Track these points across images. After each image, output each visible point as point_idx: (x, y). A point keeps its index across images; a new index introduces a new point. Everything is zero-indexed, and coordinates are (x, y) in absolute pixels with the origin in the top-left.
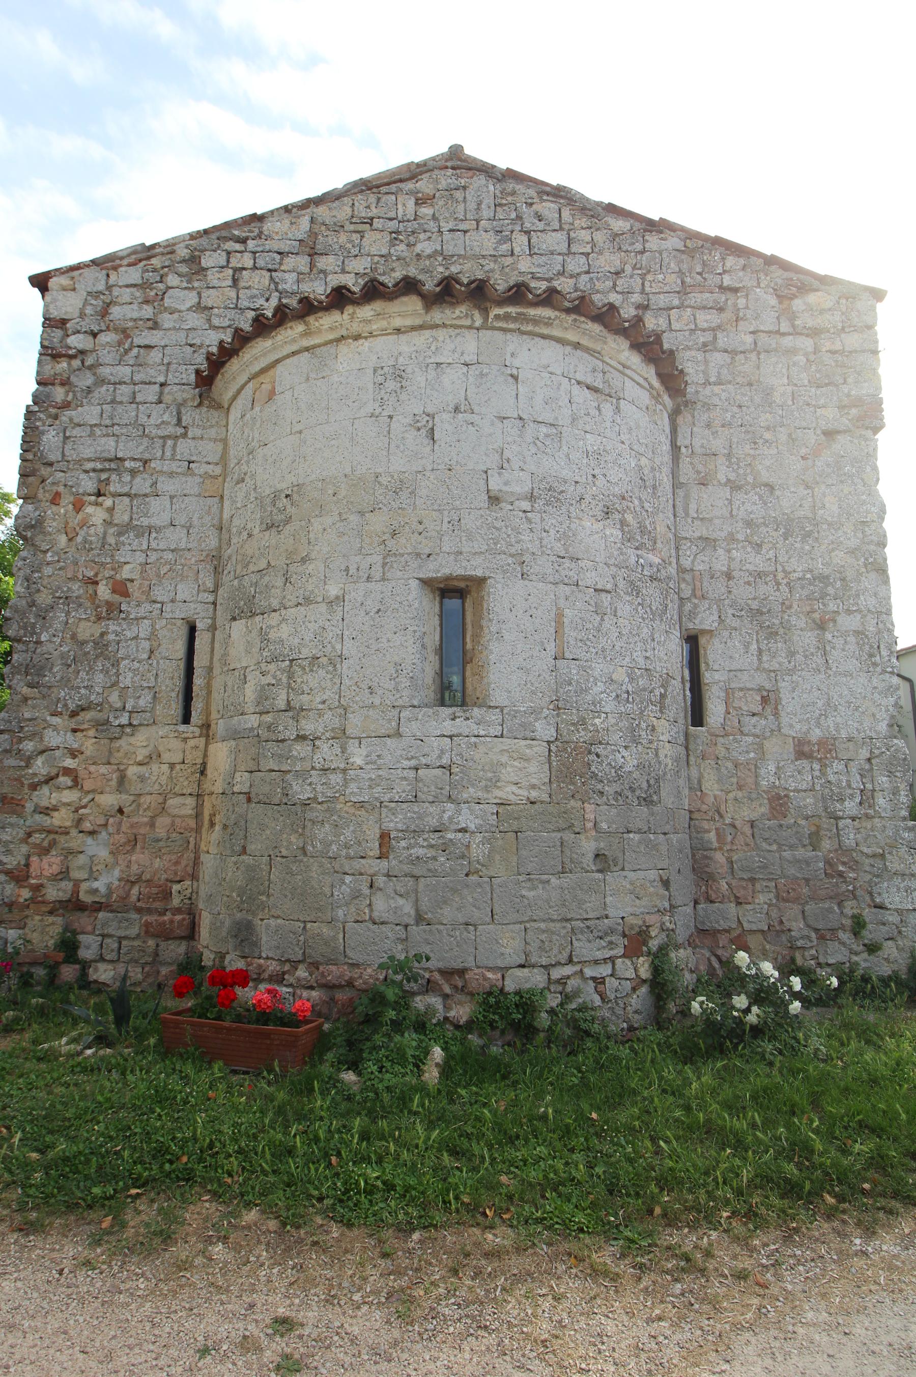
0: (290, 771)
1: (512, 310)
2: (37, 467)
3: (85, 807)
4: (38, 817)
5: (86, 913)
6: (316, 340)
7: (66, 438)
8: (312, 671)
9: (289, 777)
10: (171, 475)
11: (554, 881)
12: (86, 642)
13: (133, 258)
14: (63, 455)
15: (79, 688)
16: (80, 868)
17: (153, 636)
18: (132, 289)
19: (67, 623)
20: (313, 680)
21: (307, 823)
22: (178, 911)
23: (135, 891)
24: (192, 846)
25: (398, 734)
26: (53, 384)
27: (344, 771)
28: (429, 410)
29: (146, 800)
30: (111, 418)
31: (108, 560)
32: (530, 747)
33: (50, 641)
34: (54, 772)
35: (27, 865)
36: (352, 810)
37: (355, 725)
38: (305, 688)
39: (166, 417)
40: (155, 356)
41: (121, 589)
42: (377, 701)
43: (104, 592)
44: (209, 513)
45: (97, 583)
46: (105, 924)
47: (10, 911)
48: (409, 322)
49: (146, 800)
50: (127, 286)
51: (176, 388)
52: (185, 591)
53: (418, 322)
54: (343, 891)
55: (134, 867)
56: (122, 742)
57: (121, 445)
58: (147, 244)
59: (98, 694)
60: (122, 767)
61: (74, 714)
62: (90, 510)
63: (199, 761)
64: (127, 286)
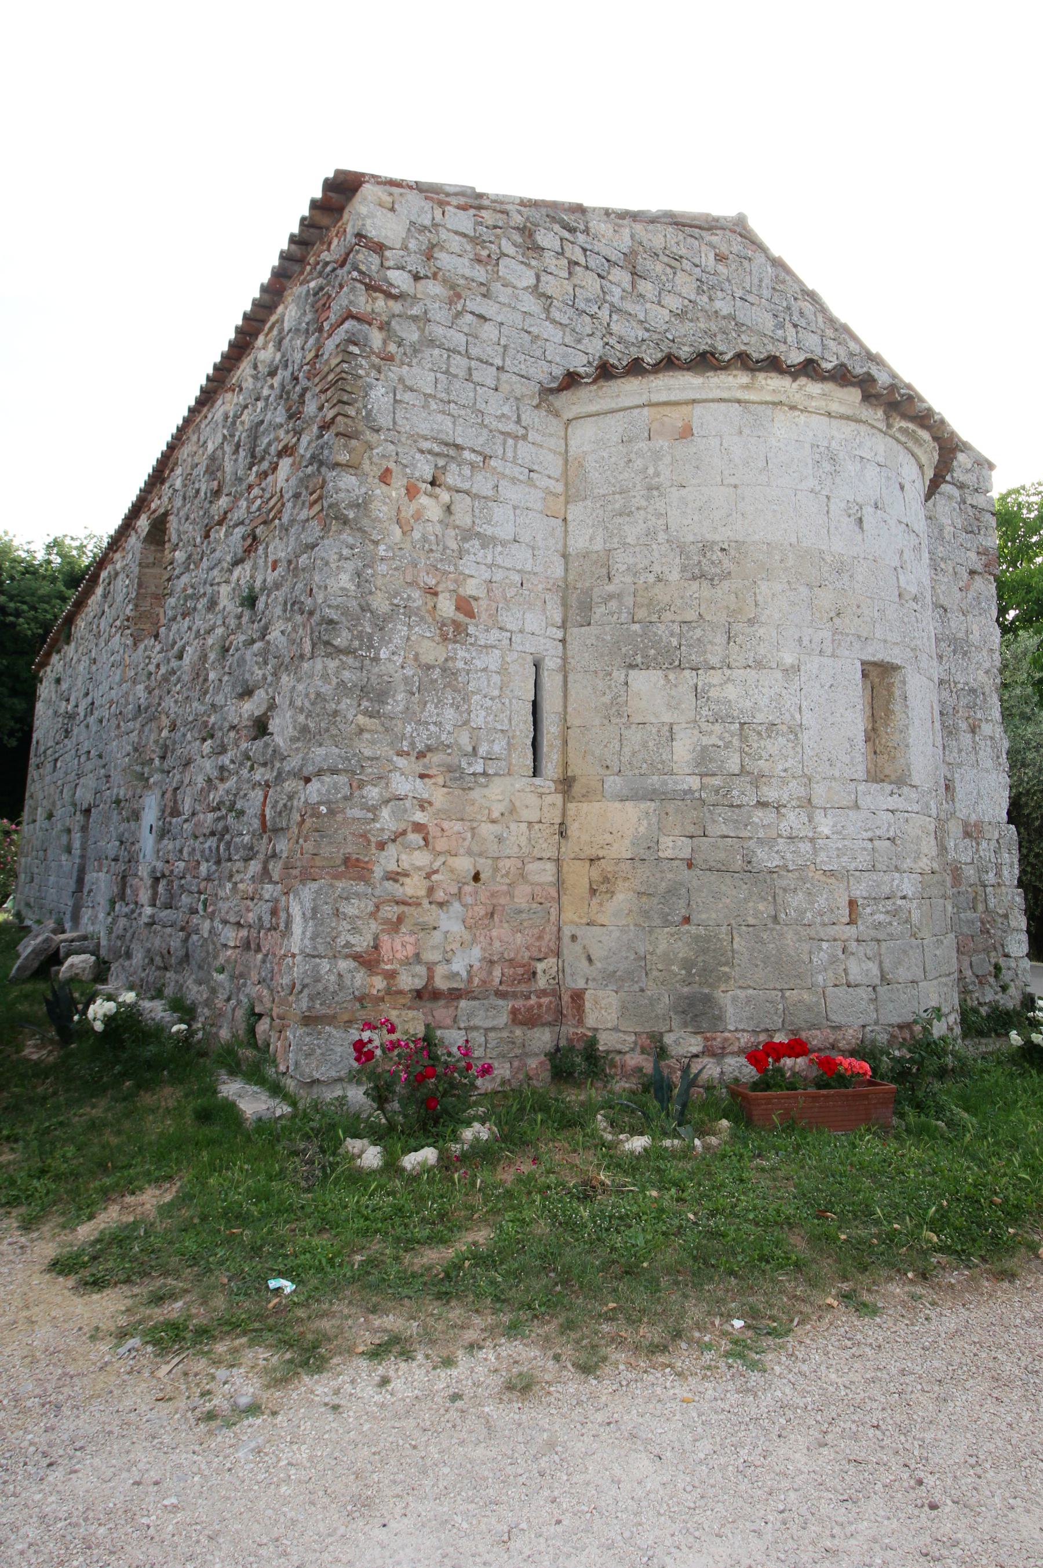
0: (750, 838)
1: (911, 426)
2: (360, 428)
3: (436, 872)
4: (389, 885)
5: (442, 1002)
6: (752, 396)
7: (396, 401)
8: (770, 737)
9: (751, 844)
10: (514, 480)
12: (433, 667)
13: (462, 201)
14: (395, 423)
15: (429, 724)
16: (434, 947)
17: (503, 670)
18: (464, 240)
19: (408, 639)
20: (774, 746)
22: (544, 993)
23: (497, 973)
24: (553, 918)
25: (857, 807)
26: (370, 324)
27: (812, 840)
28: (859, 500)
29: (505, 864)
30: (448, 391)
31: (452, 569)
33: (390, 660)
34: (402, 826)
35: (376, 947)
36: (823, 878)
37: (820, 793)
38: (763, 754)
39: (506, 410)
40: (489, 331)
41: (464, 606)
42: (837, 774)
43: (446, 607)
44: (552, 535)
45: (436, 594)
46: (470, 1016)
47: (363, 1007)
48: (843, 410)
49: (505, 864)
50: (456, 233)
51: (515, 378)
52: (533, 621)
53: (850, 412)
54: (820, 958)
55: (497, 944)
56: (475, 794)
57: (459, 429)
58: (478, 190)
59: (449, 733)
60: (475, 825)
61: (421, 755)
62: (424, 500)
63: (558, 820)
64: (456, 233)
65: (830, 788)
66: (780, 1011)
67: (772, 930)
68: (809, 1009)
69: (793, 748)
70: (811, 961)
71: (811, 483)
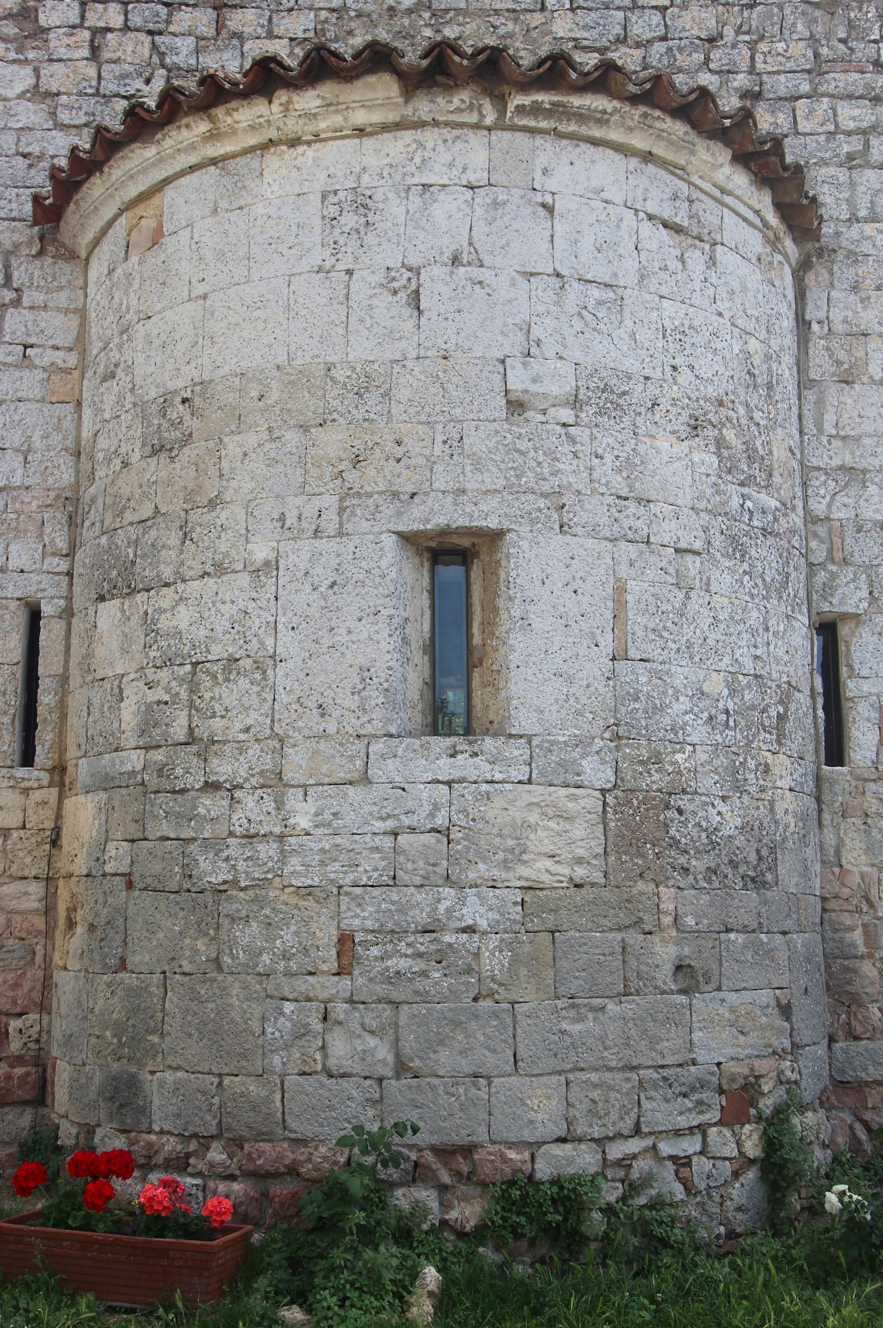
0: (194, 839)
1: (544, 98)
8: (227, 680)
9: (192, 848)
11: (612, 1007)
22: (19, 1060)
24: (39, 958)
25: (365, 780)
32: (574, 798)
36: (293, 900)
38: (217, 707)
42: (332, 729)
48: (377, 117)
53: (392, 116)
65: (316, 752)
66: (214, 1108)
67: (214, 980)
68: (255, 1108)
69: (259, 694)
70: (264, 1032)
71: (316, 258)
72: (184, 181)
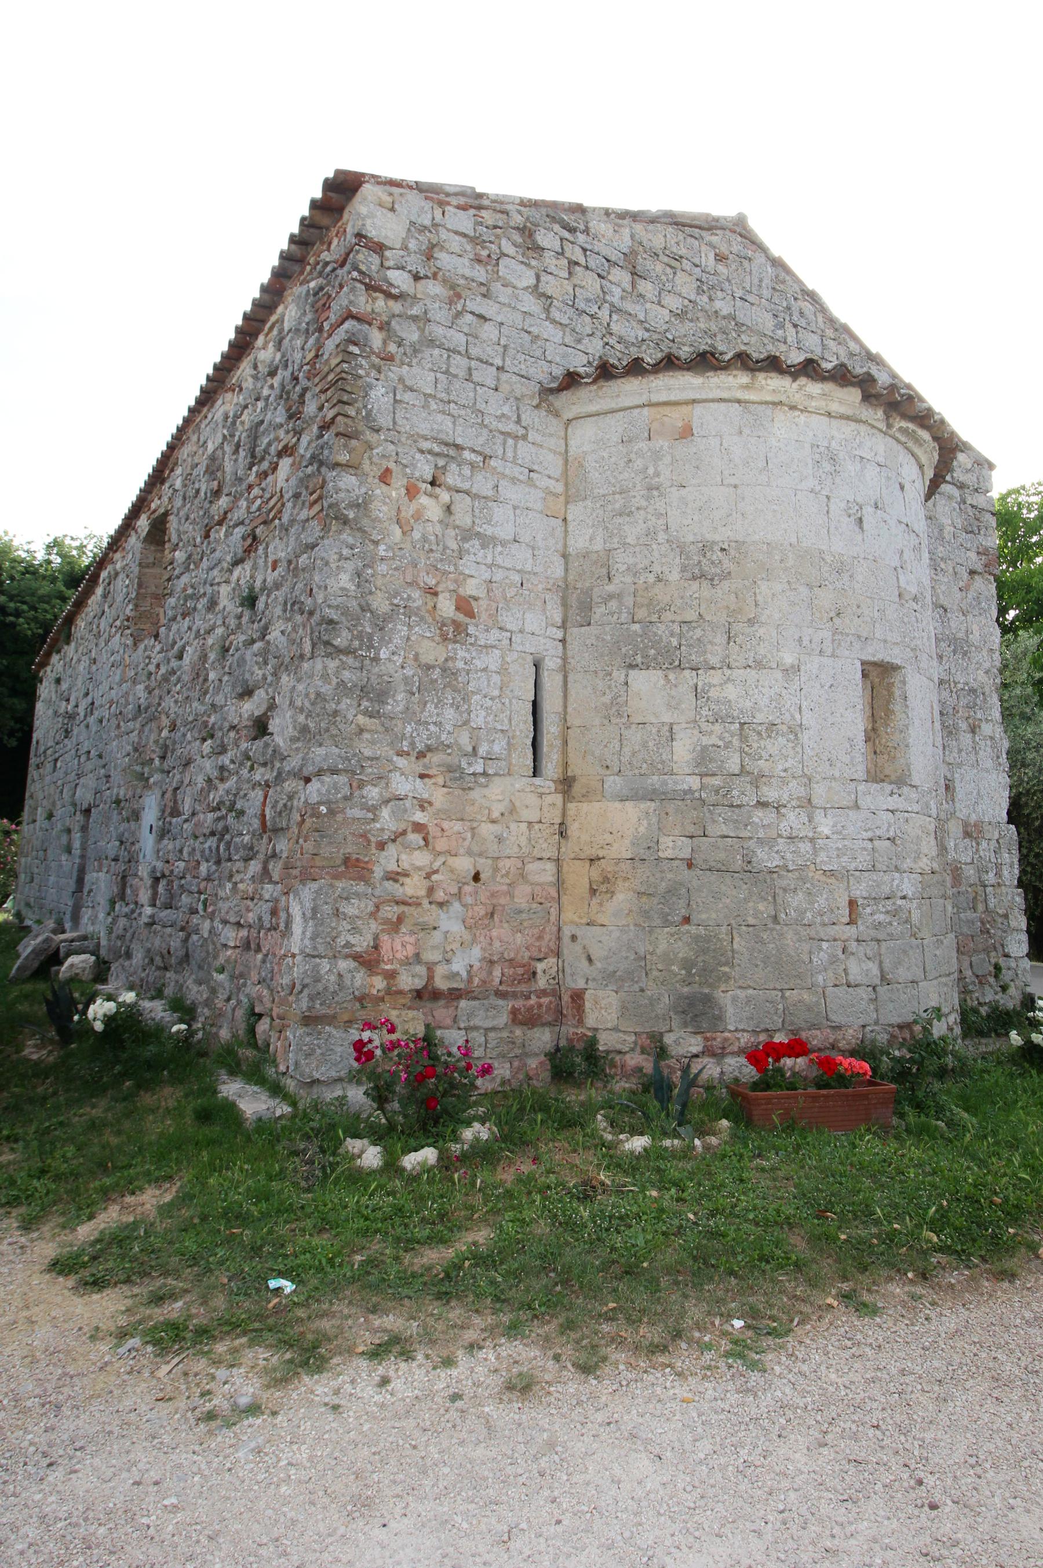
0: (751, 838)
1: (911, 426)
2: (360, 428)
3: (436, 872)
4: (389, 885)
5: (442, 1002)
6: (752, 396)
7: (396, 401)
8: (770, 737)
10: (514, 480)
12: (433, 667)
13: (462, 201)
14: (395, 423)
15: (429, 724)
16: (433, 947)
17: (503, 670)
18: (464, 240)
19: (408, 639)
20: (774, 746)
21: (780, 892)
22: (544, 993)
23: (497, 973)
24: (553, 918)
25: (857, 807)
26: (370, 324)
27: (812, 840)
28: (859, 500)
29: (505, 864)
30: (448, 391)
31: (452, 569)
33: (390, 660)
34: (402, 826)
35: (376, 947)
36: (823, 878)
37: (820, 793)
38: (763, 754)
39: (506, 410)
40: (489, 331)
41: (464, 606)
42: (837, 774)
43: (446, 607)
44: (552, 535)
45: (436, 594)
46: (470, 1016)
47: (363, 1007)
48: (843, 410)
49: (505, 864)
50: (456, 233)
51: (515, 378)
52: (533, 621)
53: (850, 413)
54: (820, 958)
55: (497, 944)
56: (475, 794)
57: (459, 429)
58: (478, 190)
59: (449, 733)
60: (475, 825)
61: (421, 755)
62: (424, 500)
63: (558, 820)
64: (456, 233)
66: (780, 1011)
67: (772, 930)
68: (809, 1009)
69: (793, 748)
70: (811, 961)
71: (811, 483)
72: (714, 406)
